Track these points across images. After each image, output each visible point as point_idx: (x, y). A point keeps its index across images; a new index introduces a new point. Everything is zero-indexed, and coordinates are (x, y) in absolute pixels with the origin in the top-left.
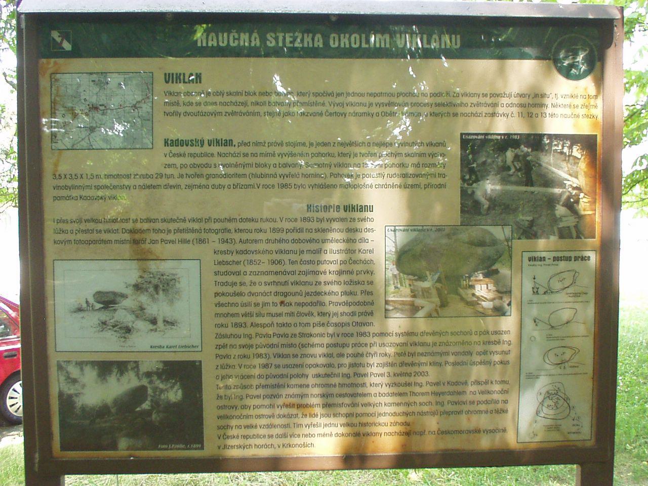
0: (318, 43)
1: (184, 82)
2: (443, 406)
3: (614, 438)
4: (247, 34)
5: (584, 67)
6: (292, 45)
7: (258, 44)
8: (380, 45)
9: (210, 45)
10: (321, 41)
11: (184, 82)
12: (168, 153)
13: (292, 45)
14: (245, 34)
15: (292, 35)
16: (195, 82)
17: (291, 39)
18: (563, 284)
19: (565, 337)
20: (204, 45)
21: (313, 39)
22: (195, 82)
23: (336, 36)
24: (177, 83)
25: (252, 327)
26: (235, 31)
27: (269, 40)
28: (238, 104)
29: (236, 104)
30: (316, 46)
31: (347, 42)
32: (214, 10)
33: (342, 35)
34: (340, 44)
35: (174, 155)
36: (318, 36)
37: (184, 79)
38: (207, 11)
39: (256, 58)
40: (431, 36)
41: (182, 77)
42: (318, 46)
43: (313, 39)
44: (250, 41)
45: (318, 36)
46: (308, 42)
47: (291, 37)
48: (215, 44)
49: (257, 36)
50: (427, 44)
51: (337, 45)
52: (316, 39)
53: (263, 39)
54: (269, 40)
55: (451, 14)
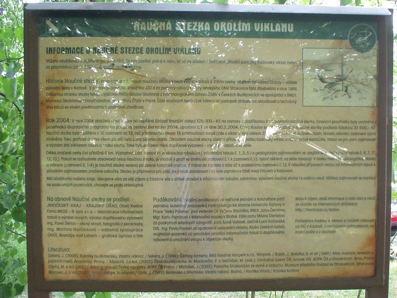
0: (169, 28)
1: (141, 53)
2: (156, 260)
3: (153, 292)
4: (164, 23)
5: (368, 44)
6: (191, 29)
7: (170, 29)
8: (281, 30)
9: (206, 30)
10: (170, 26)
11: (141, 53)
12: (221, 93)
13: (191, 29)
14: (284, 24)
15: (191, 23)
16: (194, 54)
17: (191, 26)
18: (119, 192)
19: (359, 199)
20: (164, 29)
21: (204, 25)
22: (194, 54)
23: (218, 24)
24: (49, 53)
25: (113, 207)
26: (157, 21)
27: (177, 26)
28: (64, 67)
29: (63, 67)
30: (167, 29)
31: (268, 28)
32: (194, 10)
33: (265, 24)
34: (220, 29)
35: (225, 95)
36: (169, 23)
37: (186, 51)
38: (255, 12)
39: (184, 38)
40: (275, 25)
41: (184, 51)
42: (143, 29)
43: (204, 25)
44: (204, 28)
45: (169, 23)
46: (267, 29)
47: (190, 24)
48: (145, 29)
49: (209, 25)
50: (236, 29)
51: (218, 29)
52: (206, 26)
53: (212, 27)
54: (177, 26)
55: (296, 12)
